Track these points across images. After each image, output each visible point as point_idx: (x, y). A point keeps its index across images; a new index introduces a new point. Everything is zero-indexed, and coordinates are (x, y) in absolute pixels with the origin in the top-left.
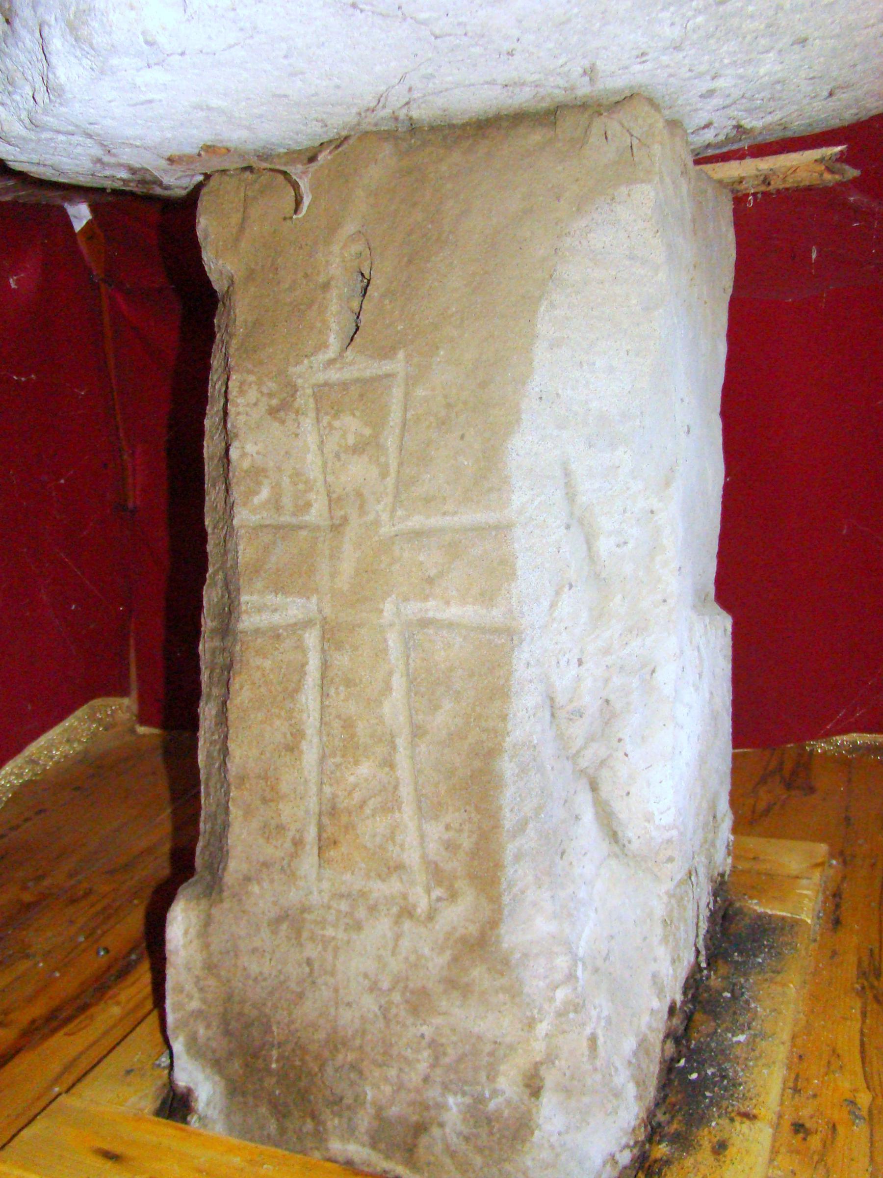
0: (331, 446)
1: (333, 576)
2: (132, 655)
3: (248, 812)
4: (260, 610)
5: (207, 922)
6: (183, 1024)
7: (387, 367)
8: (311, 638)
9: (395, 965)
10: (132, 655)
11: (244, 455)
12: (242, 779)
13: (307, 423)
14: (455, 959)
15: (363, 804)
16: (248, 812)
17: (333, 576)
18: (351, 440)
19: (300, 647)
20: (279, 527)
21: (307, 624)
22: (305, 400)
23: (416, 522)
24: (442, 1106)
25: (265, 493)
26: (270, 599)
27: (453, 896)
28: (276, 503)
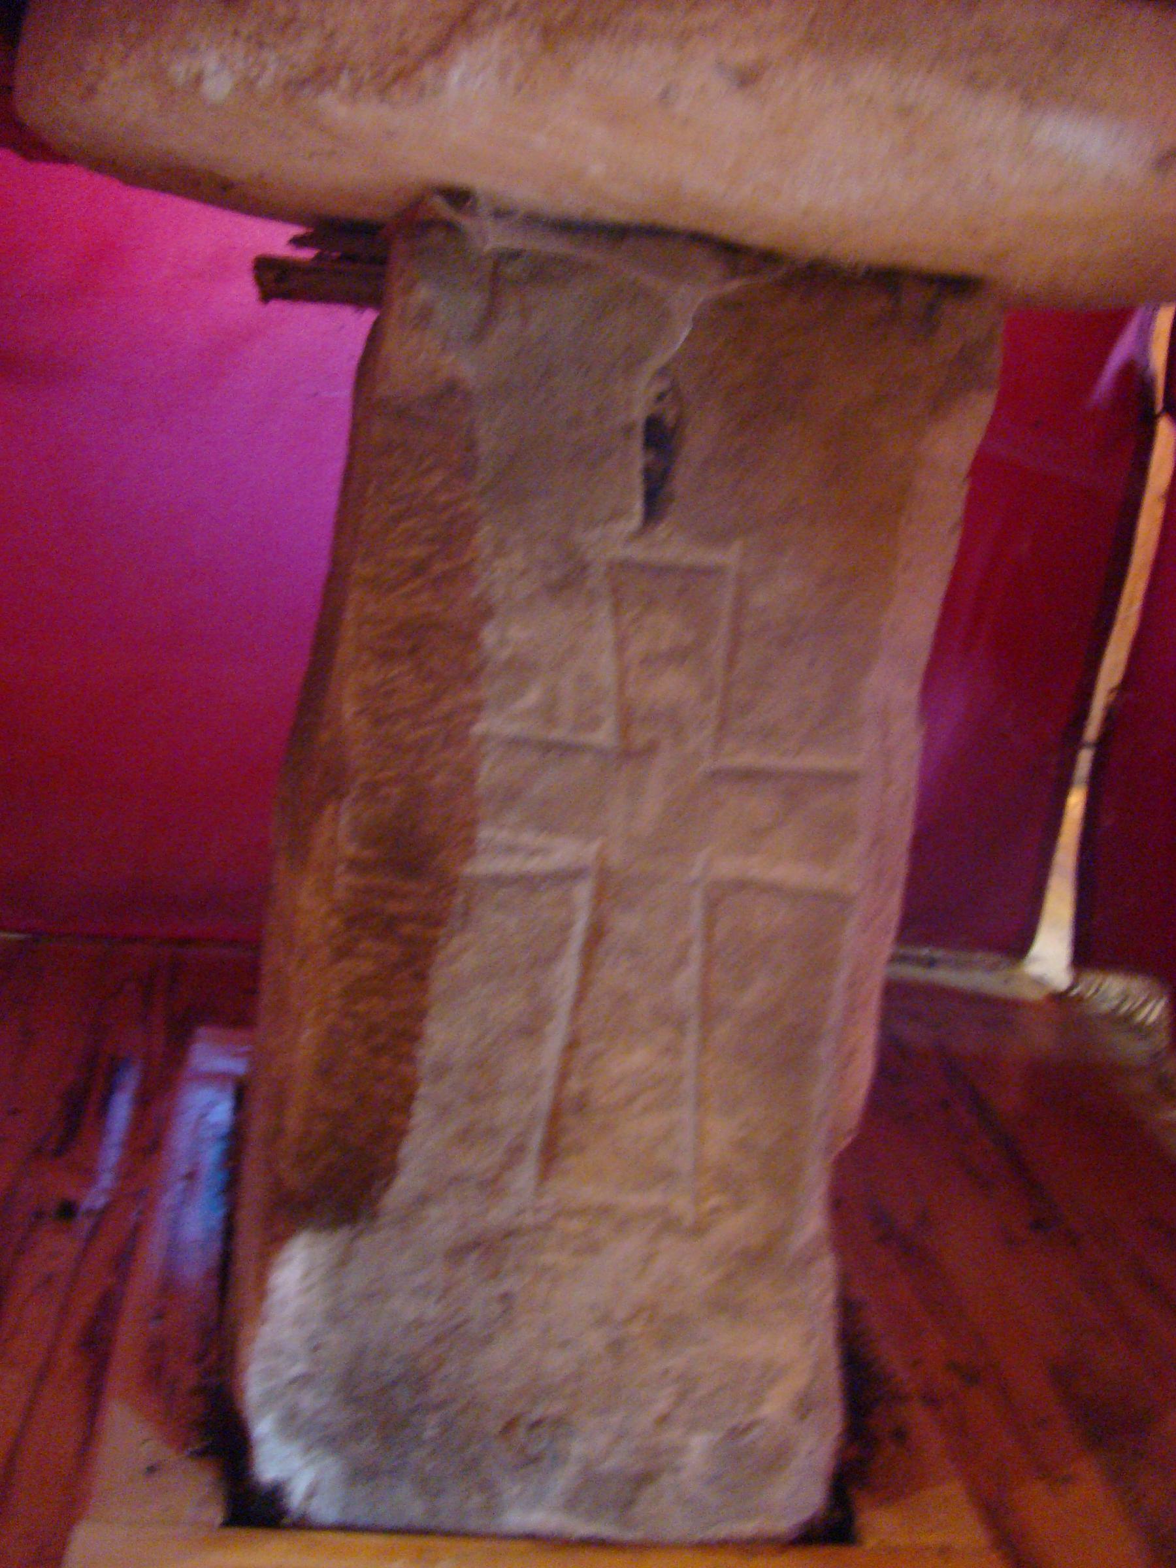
0: (638, 647)
2: (1076, 801)
5: (343, 1262)
6: (270, 1397)
7: (712, 557)
8: (583, 892)
10: (1076, 801)
11: (503, 642)
12: (441, 1070)
13: (603, 611)
14: (729, 1277)
15: (630, 1099)
16: (444, 1111)
18: (664, 645)
20: (547, 747)
22: (596, 579)
23: (748, 758)
24: (679, 1450)
25: (533, 696)
26: (528, 838)
27: (739, 1203)
28: (548, 712)
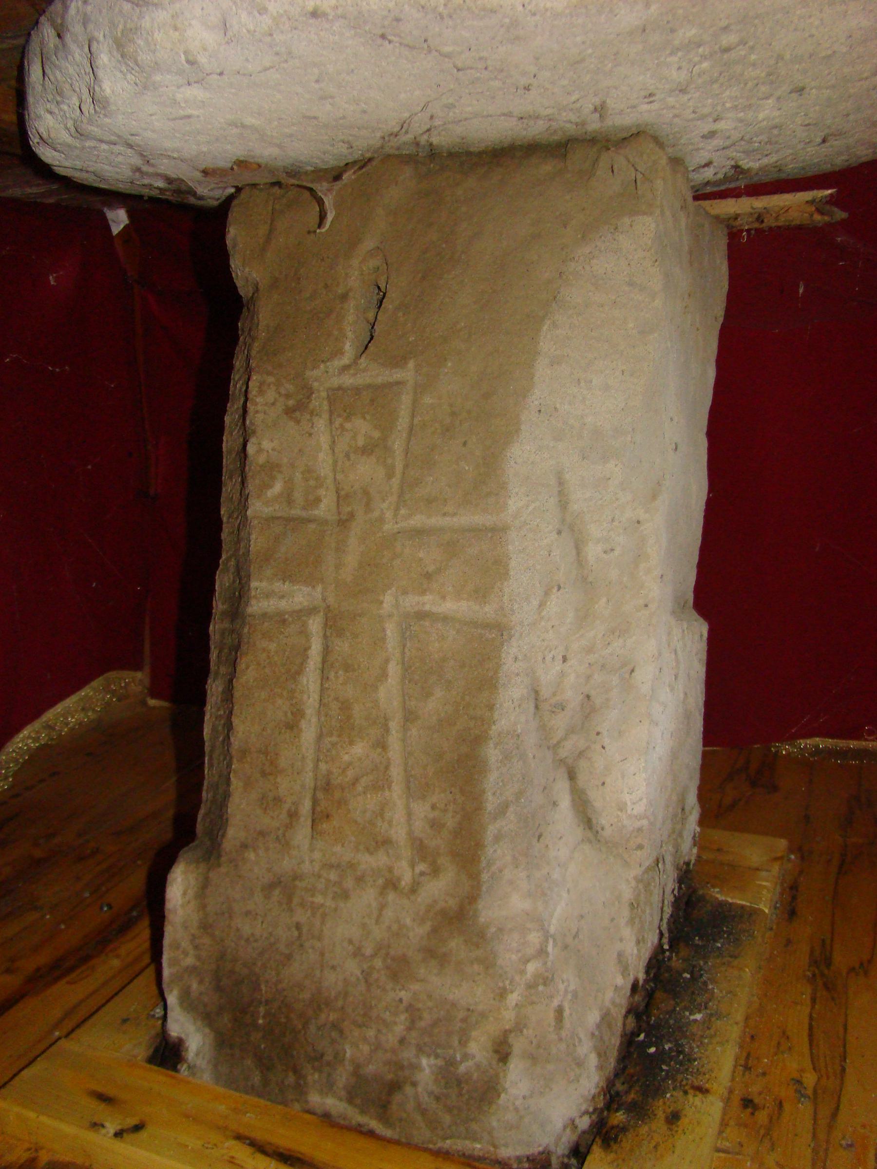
1: (338, 567)
3: (248, 784)
4: (268, 595)
8: (315, 625)
9: (378, 933)
11: (260, 450)
14: (435, 930)
17: (338, 567)
19: (304, 632)
20: (289, 520)
21: (312, 611)
25: (278, 487)
26: (278, 586)
27: (435, 871)
28: (288, 498)
